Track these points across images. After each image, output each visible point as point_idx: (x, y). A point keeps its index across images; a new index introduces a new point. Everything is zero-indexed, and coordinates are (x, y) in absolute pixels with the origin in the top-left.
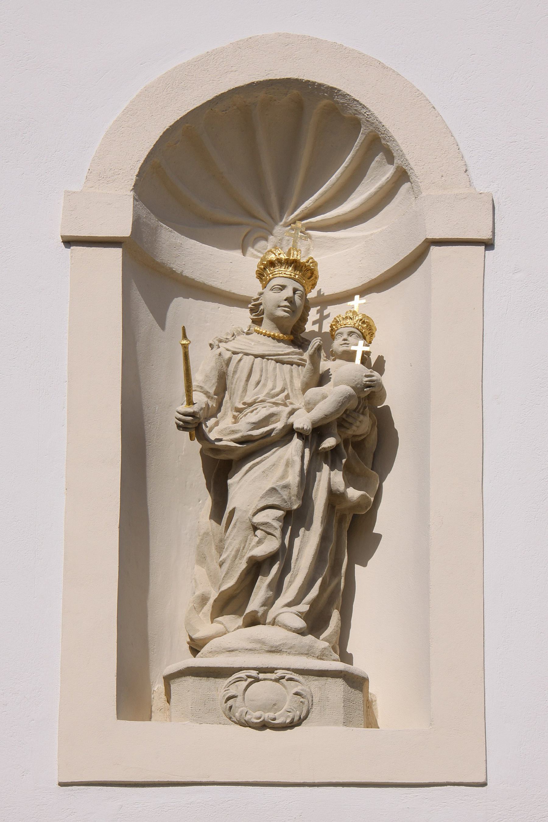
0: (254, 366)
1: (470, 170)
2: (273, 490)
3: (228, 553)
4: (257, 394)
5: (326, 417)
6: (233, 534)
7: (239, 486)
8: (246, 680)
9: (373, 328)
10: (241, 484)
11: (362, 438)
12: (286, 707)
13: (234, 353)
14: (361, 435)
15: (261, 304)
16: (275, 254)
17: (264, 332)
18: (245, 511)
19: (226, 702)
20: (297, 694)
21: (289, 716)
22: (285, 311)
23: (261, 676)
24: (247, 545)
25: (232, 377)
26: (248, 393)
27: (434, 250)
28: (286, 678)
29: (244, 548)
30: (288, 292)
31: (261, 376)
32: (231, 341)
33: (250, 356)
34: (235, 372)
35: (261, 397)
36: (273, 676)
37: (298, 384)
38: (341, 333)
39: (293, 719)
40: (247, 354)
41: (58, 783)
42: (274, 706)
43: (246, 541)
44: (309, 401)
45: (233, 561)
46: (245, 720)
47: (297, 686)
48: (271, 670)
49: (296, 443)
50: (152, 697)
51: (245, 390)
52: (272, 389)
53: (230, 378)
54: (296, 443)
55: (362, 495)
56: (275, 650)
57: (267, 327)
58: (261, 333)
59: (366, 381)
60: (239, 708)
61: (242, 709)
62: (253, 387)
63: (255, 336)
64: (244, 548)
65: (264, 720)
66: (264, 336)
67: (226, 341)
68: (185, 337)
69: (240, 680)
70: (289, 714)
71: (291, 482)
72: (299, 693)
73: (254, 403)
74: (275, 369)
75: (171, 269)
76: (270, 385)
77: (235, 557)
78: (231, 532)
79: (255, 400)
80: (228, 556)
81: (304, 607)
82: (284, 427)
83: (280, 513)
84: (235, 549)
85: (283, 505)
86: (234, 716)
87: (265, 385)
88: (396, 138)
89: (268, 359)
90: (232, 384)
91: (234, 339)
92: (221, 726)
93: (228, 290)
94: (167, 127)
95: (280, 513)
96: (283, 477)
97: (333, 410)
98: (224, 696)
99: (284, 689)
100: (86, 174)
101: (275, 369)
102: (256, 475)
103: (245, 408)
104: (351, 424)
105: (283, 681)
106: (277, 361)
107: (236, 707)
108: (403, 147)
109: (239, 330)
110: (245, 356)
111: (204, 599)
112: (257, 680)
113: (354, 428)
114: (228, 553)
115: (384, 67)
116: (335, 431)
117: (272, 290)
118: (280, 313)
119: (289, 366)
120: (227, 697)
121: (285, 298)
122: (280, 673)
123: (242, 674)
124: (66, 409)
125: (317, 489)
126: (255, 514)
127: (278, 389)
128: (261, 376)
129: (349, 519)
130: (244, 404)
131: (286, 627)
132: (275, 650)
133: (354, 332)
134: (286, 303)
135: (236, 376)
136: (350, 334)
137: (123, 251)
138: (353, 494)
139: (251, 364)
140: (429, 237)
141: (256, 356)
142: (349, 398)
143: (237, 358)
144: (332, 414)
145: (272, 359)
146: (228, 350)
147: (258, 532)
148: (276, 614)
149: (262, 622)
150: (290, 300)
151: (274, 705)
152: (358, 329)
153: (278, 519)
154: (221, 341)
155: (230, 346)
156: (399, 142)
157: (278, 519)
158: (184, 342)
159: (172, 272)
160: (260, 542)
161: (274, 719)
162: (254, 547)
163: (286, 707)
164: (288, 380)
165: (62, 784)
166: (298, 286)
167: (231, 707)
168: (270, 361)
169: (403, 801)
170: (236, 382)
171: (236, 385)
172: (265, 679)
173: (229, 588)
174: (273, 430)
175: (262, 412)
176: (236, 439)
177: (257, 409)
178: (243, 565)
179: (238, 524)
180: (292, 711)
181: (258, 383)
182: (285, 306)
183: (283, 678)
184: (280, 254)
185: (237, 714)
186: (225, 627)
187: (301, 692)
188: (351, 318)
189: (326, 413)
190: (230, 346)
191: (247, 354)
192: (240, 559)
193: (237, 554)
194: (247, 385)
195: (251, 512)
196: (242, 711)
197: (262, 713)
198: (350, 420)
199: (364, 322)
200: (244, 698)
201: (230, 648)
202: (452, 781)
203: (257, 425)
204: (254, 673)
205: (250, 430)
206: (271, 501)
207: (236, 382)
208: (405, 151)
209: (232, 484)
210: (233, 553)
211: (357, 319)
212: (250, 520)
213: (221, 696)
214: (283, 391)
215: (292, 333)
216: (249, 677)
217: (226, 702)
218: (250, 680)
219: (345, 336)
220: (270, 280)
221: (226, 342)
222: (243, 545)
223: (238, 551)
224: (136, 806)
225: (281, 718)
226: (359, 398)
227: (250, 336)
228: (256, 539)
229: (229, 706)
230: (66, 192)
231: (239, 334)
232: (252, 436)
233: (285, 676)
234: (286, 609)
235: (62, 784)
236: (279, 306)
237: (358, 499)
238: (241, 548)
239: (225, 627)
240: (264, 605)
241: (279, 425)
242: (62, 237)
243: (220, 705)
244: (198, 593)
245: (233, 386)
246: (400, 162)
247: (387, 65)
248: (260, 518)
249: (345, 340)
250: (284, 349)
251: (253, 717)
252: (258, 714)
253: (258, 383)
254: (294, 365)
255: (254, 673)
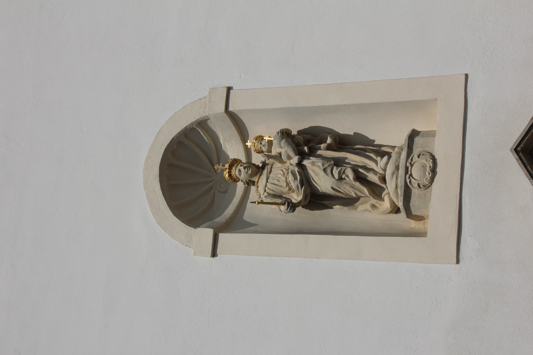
0: (271, 182)
1: (200, 98)
2: (325, 170)
3: (352, 192)
4: (283, 181)
5: (294, 150)
6: (343, 189)
7: (322, 187)
8: (411, 180)
9: (260, 136)
10: (321, 186)
11: (305, 140)
12: (425, 162)
13: (265, 191)
14: (304, 140)
15: (246, 181)
16: (226, 174)
17: (257, 179)
18: (333, 183)
19: (421, 188)
20: (419, 157)
21: (429, 160)
22: (249, 170)
23: (409, 173)
24: (348, 183)
25: (275, 192)
26: (282, 185)
27: (231, 109)
28: (410, 162)
29: (349, 184)
30: (242, 168)
31: (275, 179)
32: (260, 193)
33: (267, 184)
34: (273, 191)
35: (284, 179)
36: (410, 168)
37: (280, 165)
38: (261, 147)
39: (431, 158)
40: (266, 185)
41: (457, 265)
42: (424, 166)
43: (347, 183)
44: (287, 157)
45: (356, 189)
46: (430, 180)
47: (415, 157)
48: (407, 169)
49: (306, 162)
50: (417, 228)
51: (281, 186)
52: (281, 174)
53: (276, 193)
54: (306, 162)
55: (330, 137)
56: (397, 168)
57: (255, 179)
58: (258, 181)
59: (280, 134)
60: (424, 182)
61: (424, 181)
62: (280, 183)
63: (259, 184)
64: (349, 184)
65: (430, 171)
66: (259, 180)
67: (260, 195)
68: (255, 202)
69: (410, 182)
70: (428, 160)
71: (321, 163)
72: (418, 156)
73: (286, 182)
74: (273, 174)
75: (229, 218)
76: (280, 176)
77: (354, 188)
78: (342, 189)
79: (285, 181)
80: (353, 191)
81: (379, 159)
82: (297, 167)
83: (335, 168)
84: (350, 188)
85: (331, 166)
86: (428, 185)
87: (279, 178)
88: (185, 126)
89: (269, 177)
90: (278, 192)
91: (260, 192)
92: (432, 191)
93: (240, 198)
94: (173, 215)
95: (335, 168)
96: (319, 167)
97: (291, 148)
98: (418, 189)
99: (416, 163)
100: (188, 247)
101: (273, 174)
102: (317, 179)
103: (289, 186)
104: (298, 141)
105: (412, 163)
106: (270, 173)
107: (424, 184)
108: (189, 123)
109: (256, 190)
110: (267, 186)
111: (373, 206)
112: (411, 175)
113: (300, 141)
114: (352, 192)
115: (159, 132)
116: (300, 148)
117: (240, 175)
118: (250, 172)
119: (272, 169)
120: (418, 188)
121: (244, 170)
122: (408, 164)
123: (408, 181)
124: (283, 258)
125: (326, 155)
126: (334, 178)
127: (282, 173)
128: (275, 179)
129: (340, 146)
130: (287, 187)
131: (387, 163)
132: (397, 168)
133: (260, 142)
134: (246, 169)
135: (275, 190)
136: (261, 144)
137: (220, 233)
138: (329, 141)
139: (270, 184)
140: (224, 111)
141: (267, 181)
142: (287, 141)
143: (267, 190)
144: (293, 148)
145: (269, 175)
146: (264, 194)
147: (343, 176)
148: (380, 169)
149: (384, 175)
150: (245, 168)
151: (423, 166)
152: (259, 141)
153: (337, 169)
154: (260, 197)
155: (262, 194)
156: (187, 125)
157: (337, 169)
158: (257, 203)
159: (230, 218)
160: (347, 176)
161: (430, 167)
162: (349, 179)
163: (425, 162)
164: (278, 169)
165: (458, 262)
166: (240, 165)
167: (423, 186)
168: (270, 176)
169: (473, 110)
170: (277, 190)
171: (278, 191)
172: (411, 171)
173: (368, 191)
174: (298, 171)
175: (290, 178)
176: (301, 187)
177: (289, 181)
178: (357, 184)
179: (338, 186)
180: (426, 159)
181: (278, 181)
182: (247, 169)
183: (410, 163)
184: (226, 172)
185: (427, 183)
186: (386, 194)
187: (418, 155)
188: (254, 144)
189: (292, 150)
190: (262, 194)
191: (266, 185)
192: (355, 186)
193: (353, 187)
194: (279, 185)
195: (333, 180)
196: (426, 181)
197: (427, 172)
198: (296, 142)
199: (257, 139)
200: (419, 180)
201: (395, 188)
202: (464, 88)
203: (295, 178)
204: (408, 176)
205: (297, 181)
206: (329, 171)
207: (277, 190)
208: (190, 123)
209: (321, 190)
210: (352, 189)
211: (255, 142)
212: (337, 180)
213: (418, 191)
214: (282, 170)
215: (259, 169)
216: (409, 178)
217: (421, 188)
218: (411, 178)
219: (262, 146)
220: (236, 176)
221: (261, 195)
222: (348, 184)
223: (351, 187)
224: (470, 229)
225: (430, 163)
226: (287, 138)
227: (259, 186)
228: (346, 178)
229: (422, 187)
230: (194, 255)
231: (258, 190)
232: (300, 180)
233: (410, 162)
234: (379, 165)
235: (458, 262)
236: (247, 172)
237: (331, 139)
238: (350, 185)
239: (386, 194)
240: (376, 175)
241: (296, 169)
242: (211, 257)
243: (422, 191)
244: (370, 209)
245: (279, 192)
246: (195, 125)
247: (158, 131)
248: (336, 176)
249: (263, 146)
250: (265, 171)
251: (428, 176)
252: (427, 174)
253: (278, 181)
254: (272, 167)
255: (408, 176)
